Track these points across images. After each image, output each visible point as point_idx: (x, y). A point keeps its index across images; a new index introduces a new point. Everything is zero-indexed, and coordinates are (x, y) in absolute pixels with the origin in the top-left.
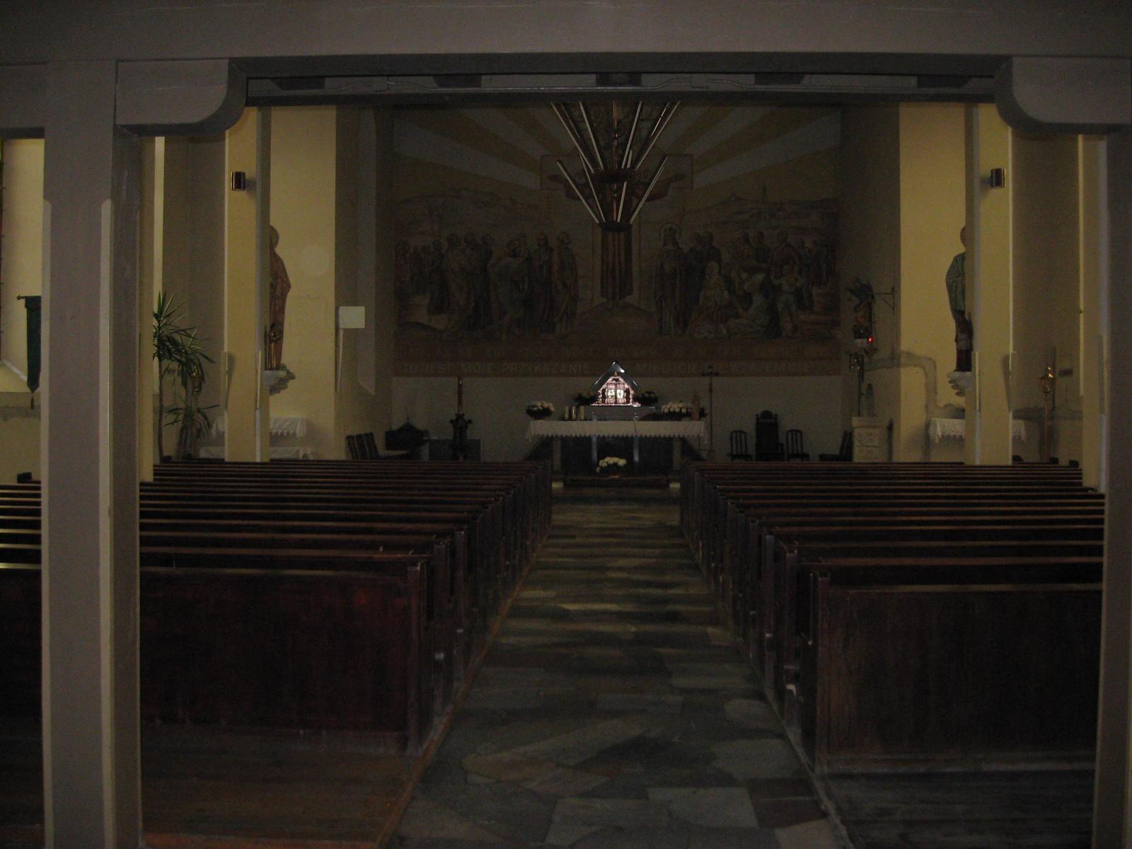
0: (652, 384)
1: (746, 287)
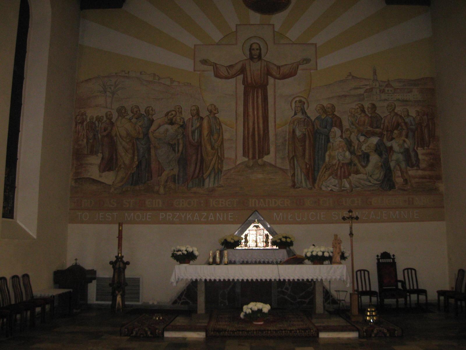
0: (283, 230)
1: (364, 148)
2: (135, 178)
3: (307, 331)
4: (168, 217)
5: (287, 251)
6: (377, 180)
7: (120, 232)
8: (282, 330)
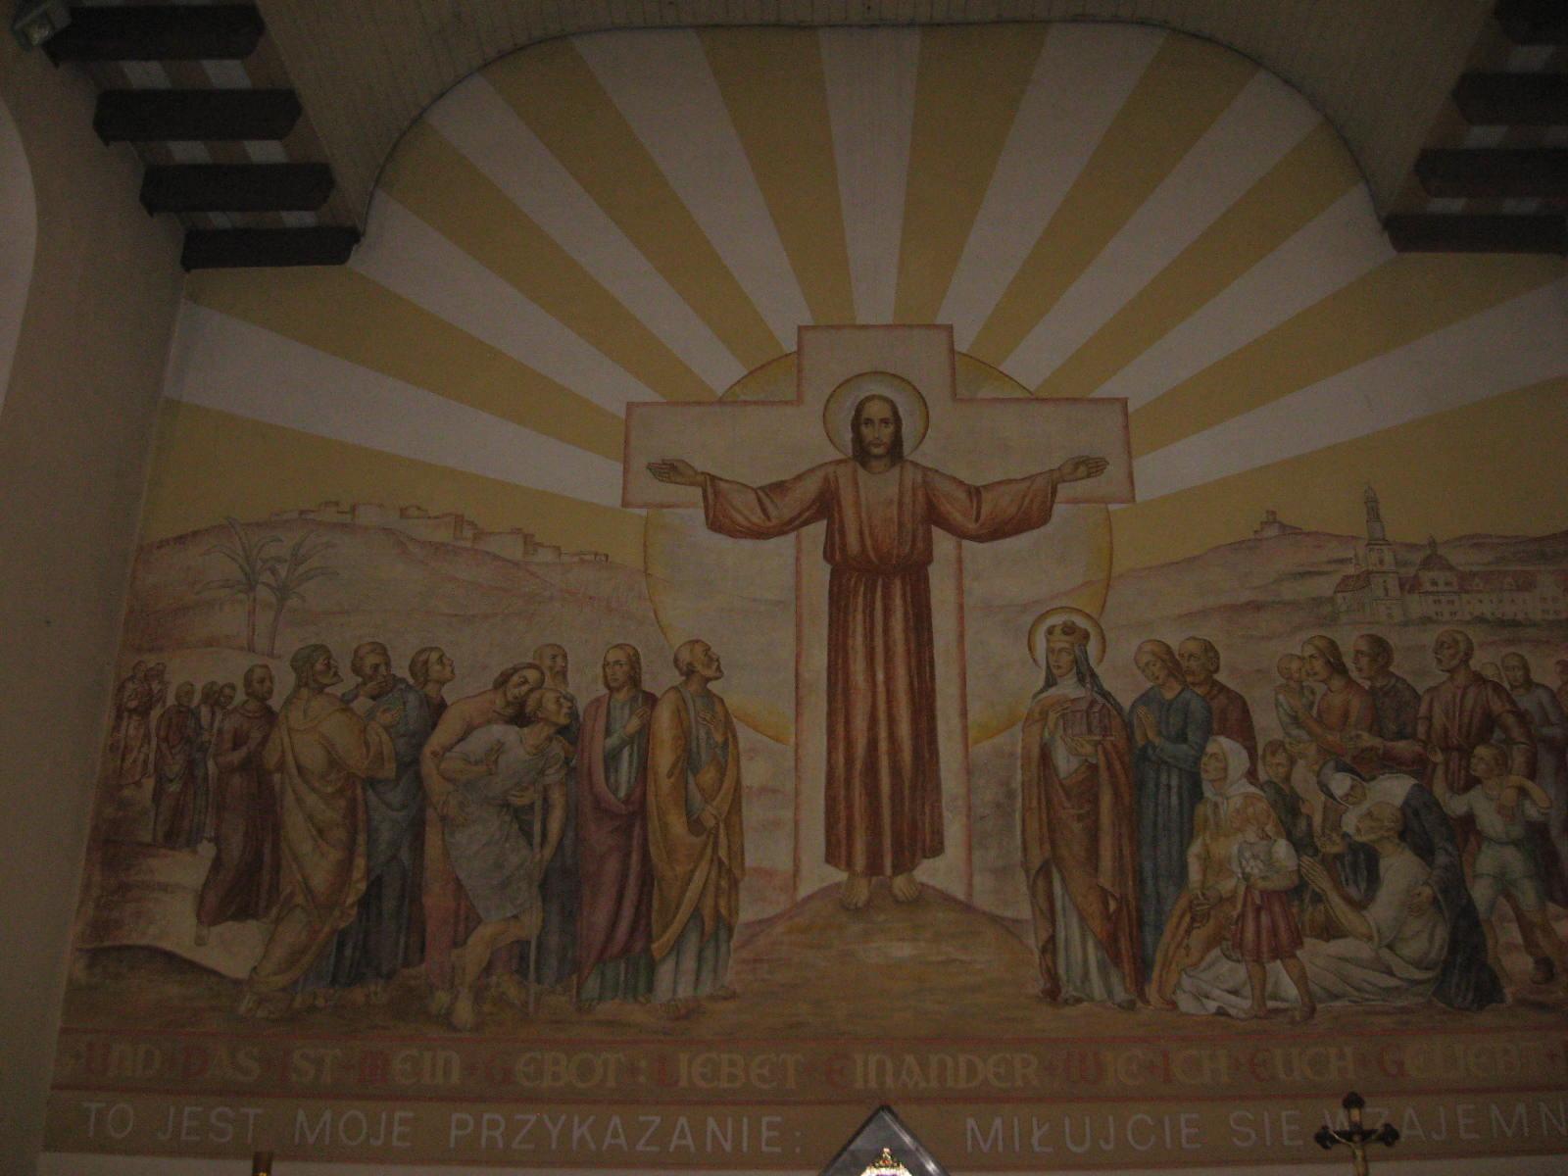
1: (1350, 822)
2: (348, 952)
4: (485, 1133)
6: (1418, 964)
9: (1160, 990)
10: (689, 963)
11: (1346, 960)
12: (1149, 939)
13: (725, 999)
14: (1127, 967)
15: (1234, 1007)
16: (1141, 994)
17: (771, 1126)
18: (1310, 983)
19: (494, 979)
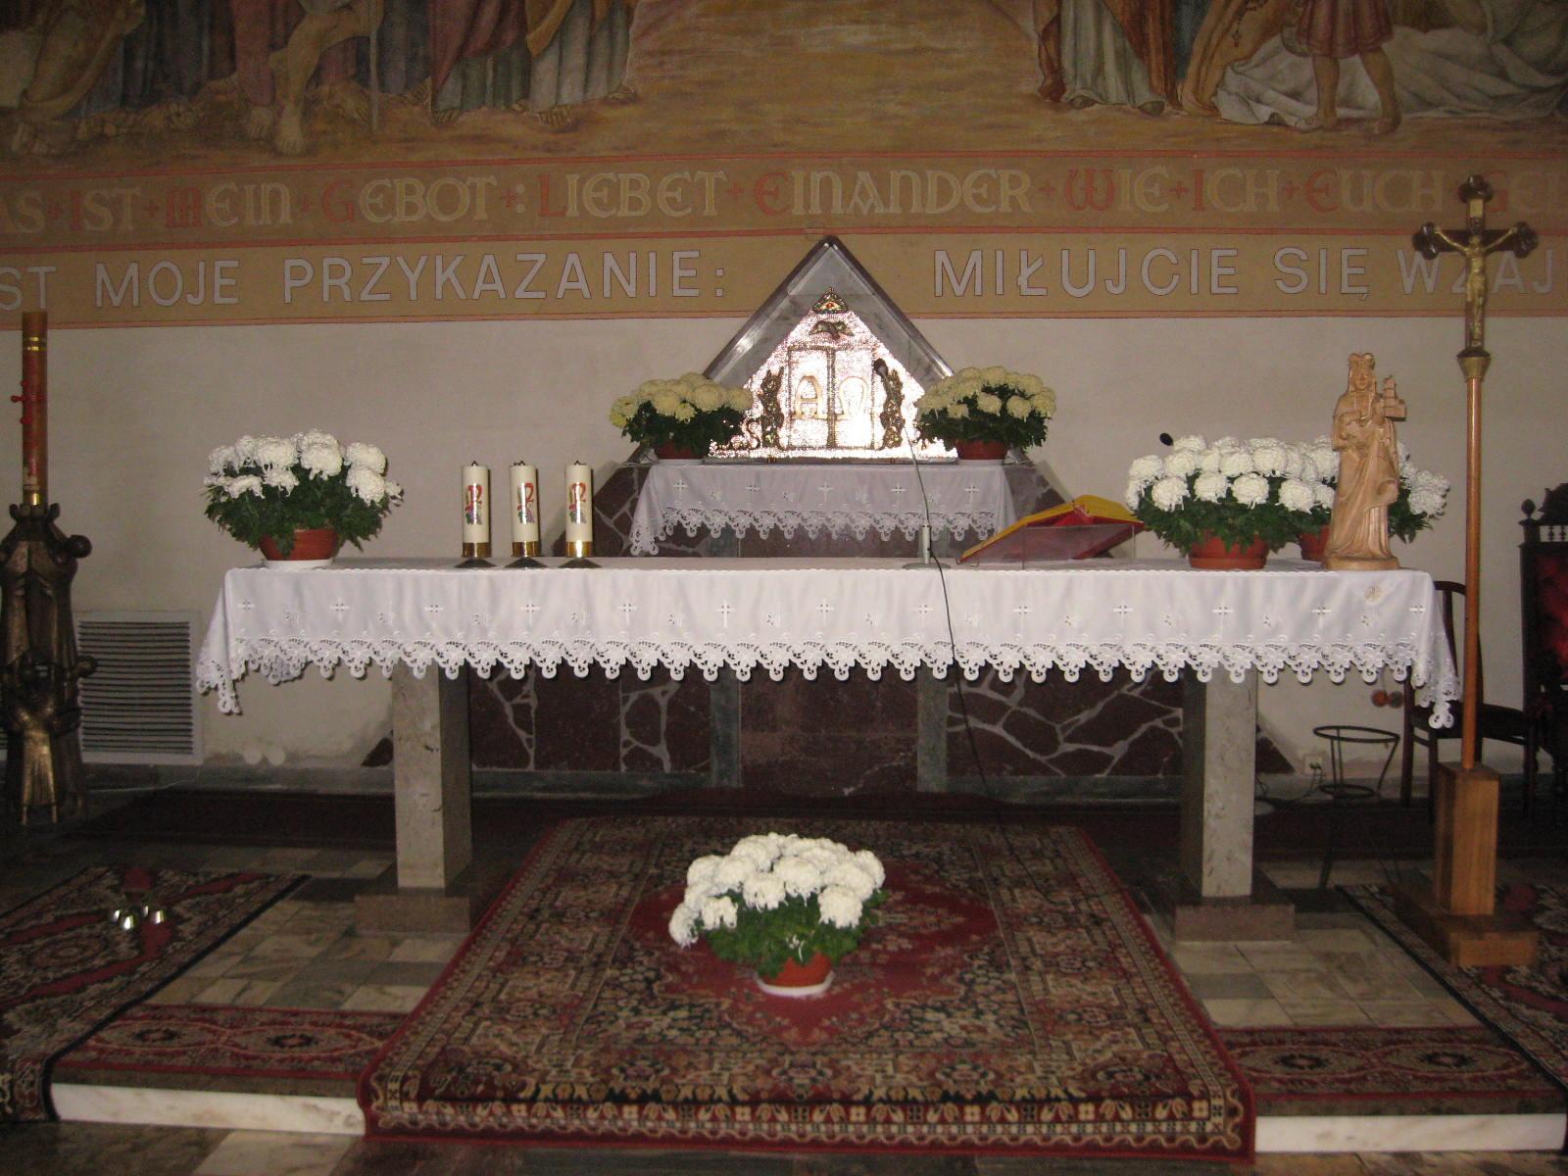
2: (139, 65)
3: (1161, 1113)
4: (327, 282)
5: (1007, 473)
6: (1540, 66)
7: (34, 370)
8: (960, 1101)
9: (1195, 92)
10: (576, 58)
11: (1448, 57)
12: (1186, 23)
13: (623, 103)
14: (1156, 59)
15: (1292, 114)
16: (1172, 96)
17: (685, 264)
18: (1397, 88)
19: (325, 89)
